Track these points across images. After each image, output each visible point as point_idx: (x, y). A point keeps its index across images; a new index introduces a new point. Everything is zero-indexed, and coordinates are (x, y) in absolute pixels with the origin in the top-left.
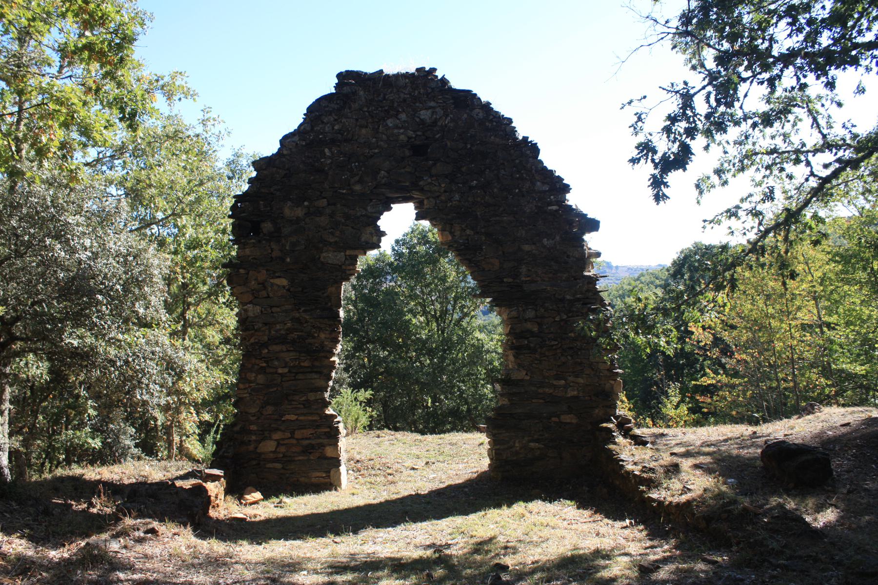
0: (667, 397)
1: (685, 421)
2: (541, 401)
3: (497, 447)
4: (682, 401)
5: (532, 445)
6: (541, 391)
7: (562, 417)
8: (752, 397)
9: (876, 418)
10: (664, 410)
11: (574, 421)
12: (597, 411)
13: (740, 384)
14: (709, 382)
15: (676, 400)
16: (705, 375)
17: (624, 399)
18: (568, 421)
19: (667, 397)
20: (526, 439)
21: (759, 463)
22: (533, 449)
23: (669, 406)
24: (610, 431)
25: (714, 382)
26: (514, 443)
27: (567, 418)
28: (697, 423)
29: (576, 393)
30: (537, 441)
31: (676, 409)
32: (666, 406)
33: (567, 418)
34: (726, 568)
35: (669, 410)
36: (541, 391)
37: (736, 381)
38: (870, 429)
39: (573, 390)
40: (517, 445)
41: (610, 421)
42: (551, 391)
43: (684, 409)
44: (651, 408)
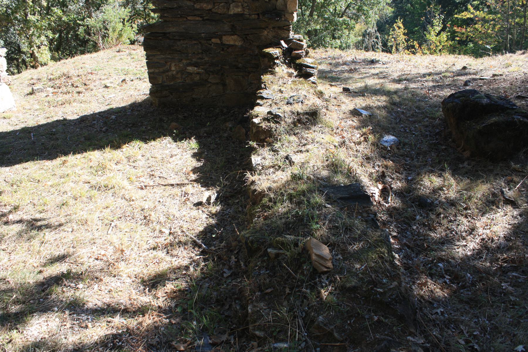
0: (432, 26)
1: (443, 46)
2: (197, 19)
3: (152, 70)
4: (443, 30)
5: (190, 69)
6: (197, 6)
7: (224, 38)
8: (499, 30)
9: (1, 166)
10: (428, 36)
11: (239, 43)
12: (266, 32)
13: (493, 20)
14: (468, 16)
15: (438, 29)
16: (467, 9)
17: (401, 25)
18: (232, 43)
19: (432, 26)
20: (185, 62)
21: (440, 113)
22: (191, 74)
23: (433, 33)
24: (271, 58)
25: (472, 16)
26: (170, 67)
27: (231, 40)
28: (452, 50)
29: (239, 10)
30: (196, 65)
31: (437, 36)
32: (430, 33)
33: (231, 40)
34: (504, 197)
35: (432, 37)
36: (197, 6)
37: (491, 17)
38: (500, 102)
39: (237, 7)
40: (173, 68)
41: (277, 45)
42: (210, 7)
43: (444, 36)
44: (143, 30)
